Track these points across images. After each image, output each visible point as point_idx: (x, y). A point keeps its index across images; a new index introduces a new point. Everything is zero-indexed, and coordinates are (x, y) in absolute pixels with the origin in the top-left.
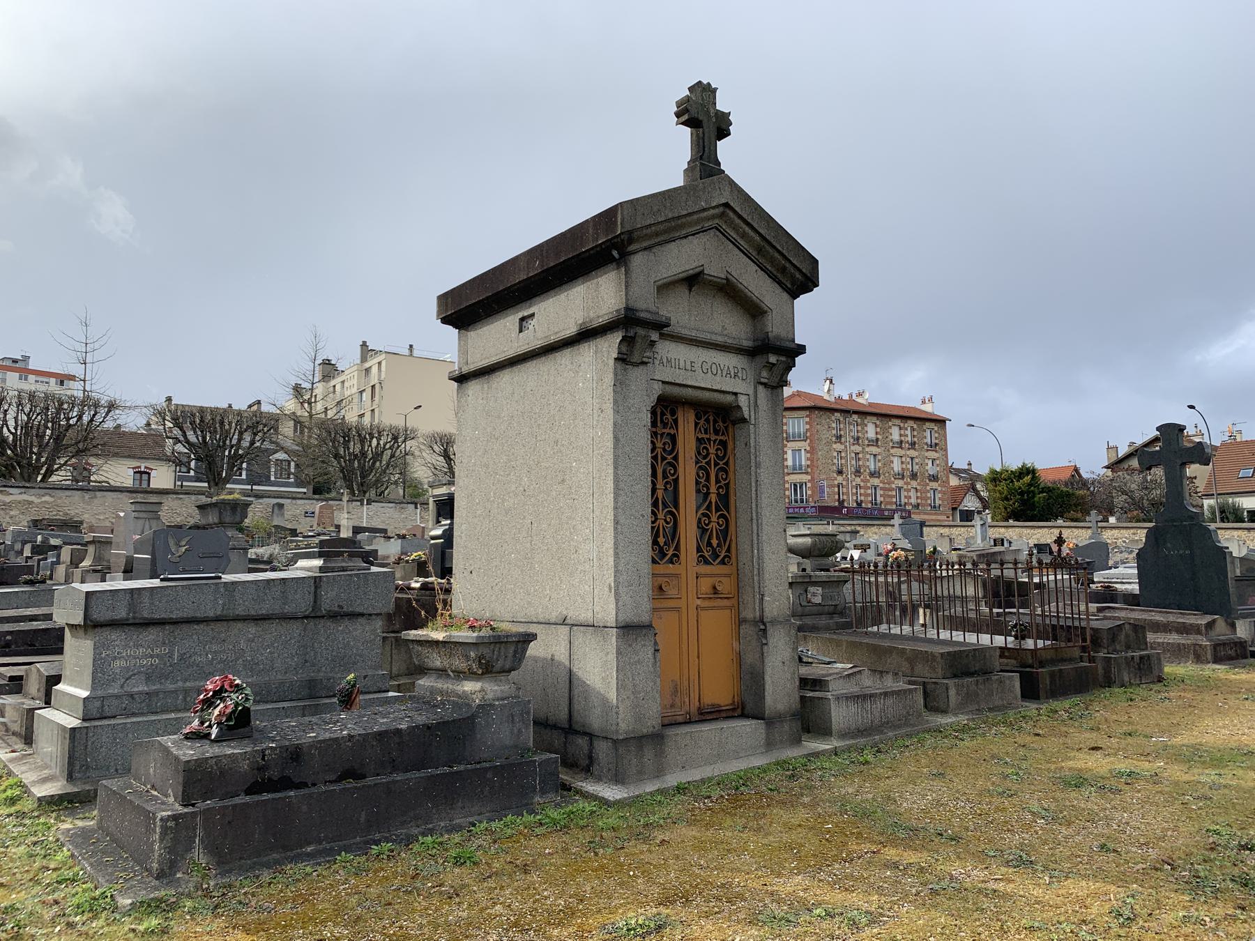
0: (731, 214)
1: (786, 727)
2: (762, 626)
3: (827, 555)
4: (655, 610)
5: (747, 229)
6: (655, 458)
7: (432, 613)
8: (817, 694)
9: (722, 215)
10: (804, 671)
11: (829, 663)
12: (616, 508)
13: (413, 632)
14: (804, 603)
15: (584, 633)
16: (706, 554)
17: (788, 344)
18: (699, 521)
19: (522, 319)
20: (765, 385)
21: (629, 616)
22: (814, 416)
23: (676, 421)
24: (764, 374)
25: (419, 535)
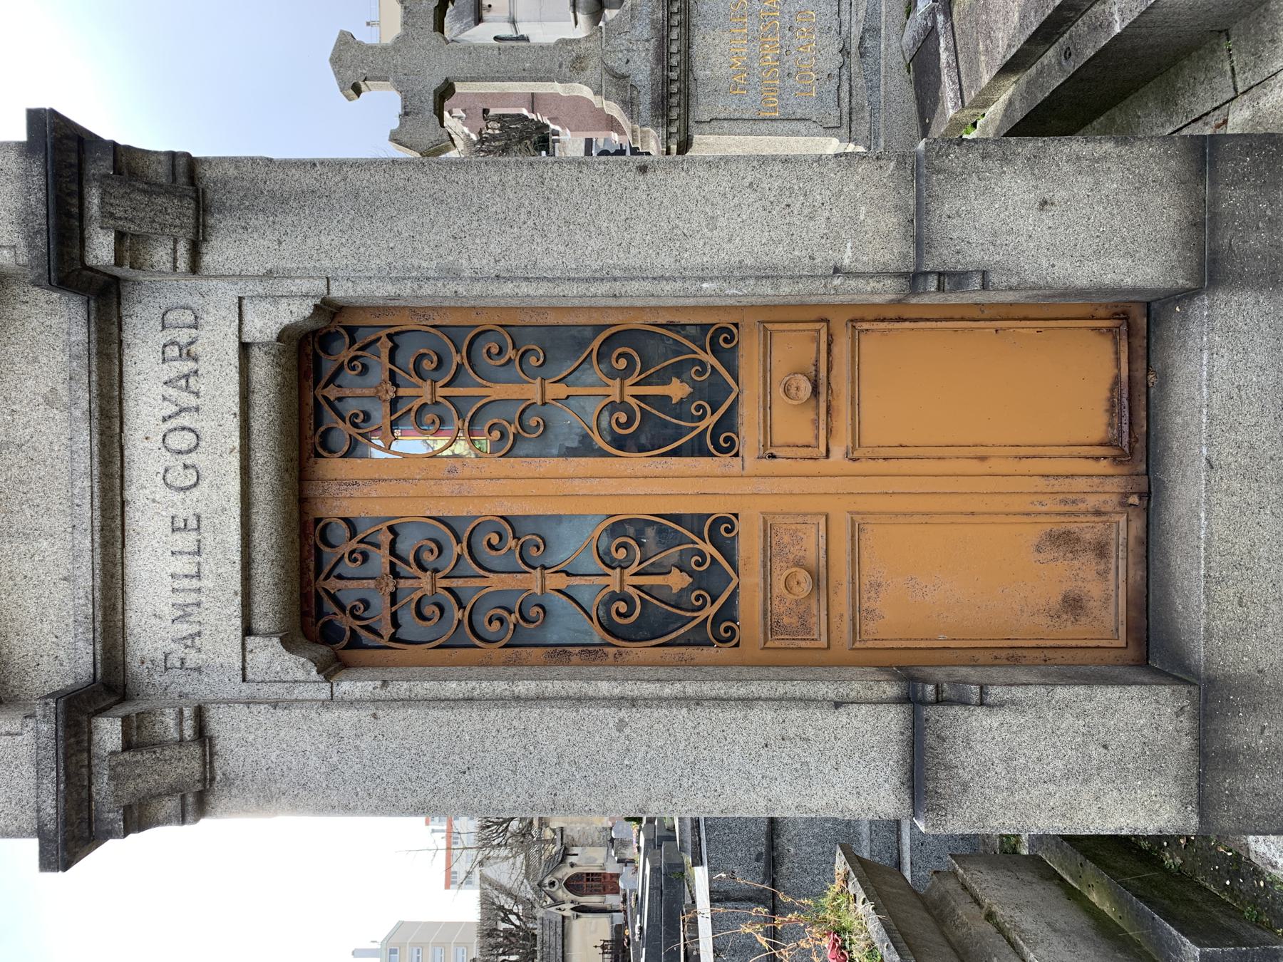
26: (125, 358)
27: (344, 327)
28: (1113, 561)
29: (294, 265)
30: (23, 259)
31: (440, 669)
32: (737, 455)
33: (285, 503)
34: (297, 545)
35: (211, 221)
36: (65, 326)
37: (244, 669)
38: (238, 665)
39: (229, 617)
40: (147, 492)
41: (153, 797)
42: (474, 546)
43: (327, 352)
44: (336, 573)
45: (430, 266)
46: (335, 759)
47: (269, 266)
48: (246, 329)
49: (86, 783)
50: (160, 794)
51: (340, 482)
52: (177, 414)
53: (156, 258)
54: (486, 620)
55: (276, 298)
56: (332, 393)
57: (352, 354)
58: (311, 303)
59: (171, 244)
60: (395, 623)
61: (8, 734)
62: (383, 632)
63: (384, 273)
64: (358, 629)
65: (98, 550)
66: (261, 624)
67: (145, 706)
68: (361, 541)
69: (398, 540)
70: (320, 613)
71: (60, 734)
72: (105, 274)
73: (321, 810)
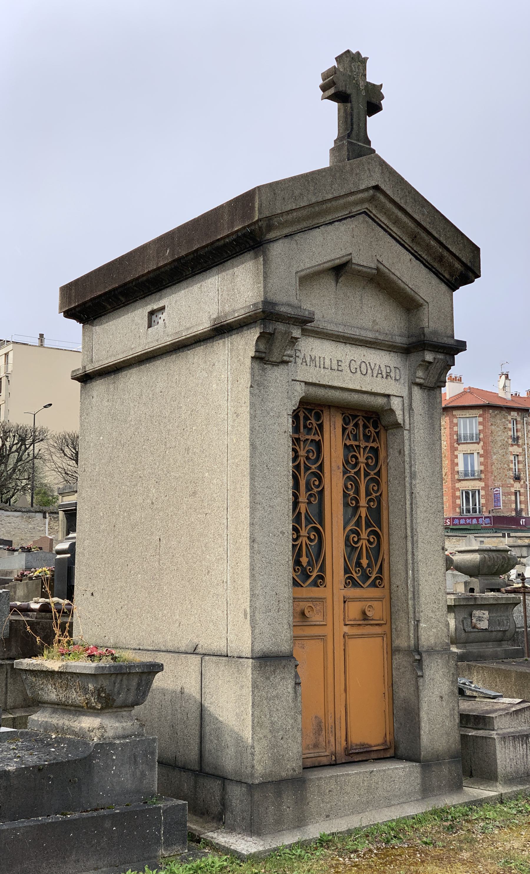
0: (382, 198)
1: (445, 770)
2: (417, 656)
3: (497, 573)
4: (296, 638)
5: (400, 214)
6: (297, 467)
7: (49, 639)
8: (481, 733)
9: (372, 199)
10: (465, 706)
11: (494, 697)
12: (252, 524)
13: (27, 661)
14: (469, 629)
15: (217, 664)
16: (355, 576)
17: (446, 340)
18: (347, 539)
19: (152, 313)
20: (420, 385)
21: (266, 645)
22: (487, 415)
23: (321, 426)
24: (420, 373)
25: (46, 549)
26: (386, 352)
28: (312, 751)
32: (345, 587)
35: (426, 391)
39: (312, 377)
48: (394, 397)
58: (402, 423)
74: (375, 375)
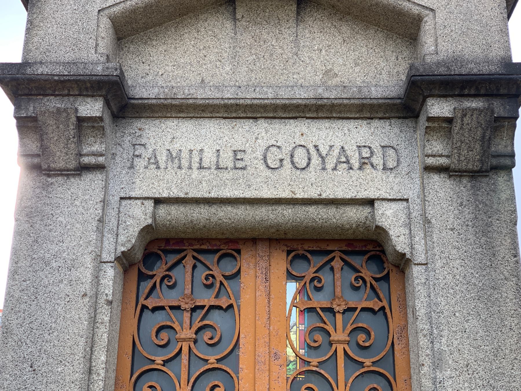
26: (360, 121)
27: (388, 273)
29: (435, 240)
30: (428, 59)
31: (116, 345)
33: (253, 229)
34: (220, 237)
35: (465, 181)
36: (381, 83)
37: (130, 198)
38: (133, 194)
40: (263, 134)
41: (41, 136)
42: (214, 373)
43: (369, 259)
44: (198, 264)
45: (443, 344)
46: (54, 265)
47: (433, 221)
49: (57, 93)
50: (42, 140)
51: (268, 269)
52: (320, 155)
53: (434, 143)
54: (153, 384)
55: (409, 225)
56: (337, 264)
57: (368, 279)
58: (407, 251)
59: (445, 153)
60: (155, 309)
61: (97, 45)
62: (149, 300)
63: (434, 308)
64: (153, 281)
65: (222, 102)
66: (162, 210)
67: (108, 131)
68: (221, 283)
69: (221, 311)
70: (167, 252)
71: (94, 78)
72: (420, 110)
73: (16, 253)
74: (330, 166)
